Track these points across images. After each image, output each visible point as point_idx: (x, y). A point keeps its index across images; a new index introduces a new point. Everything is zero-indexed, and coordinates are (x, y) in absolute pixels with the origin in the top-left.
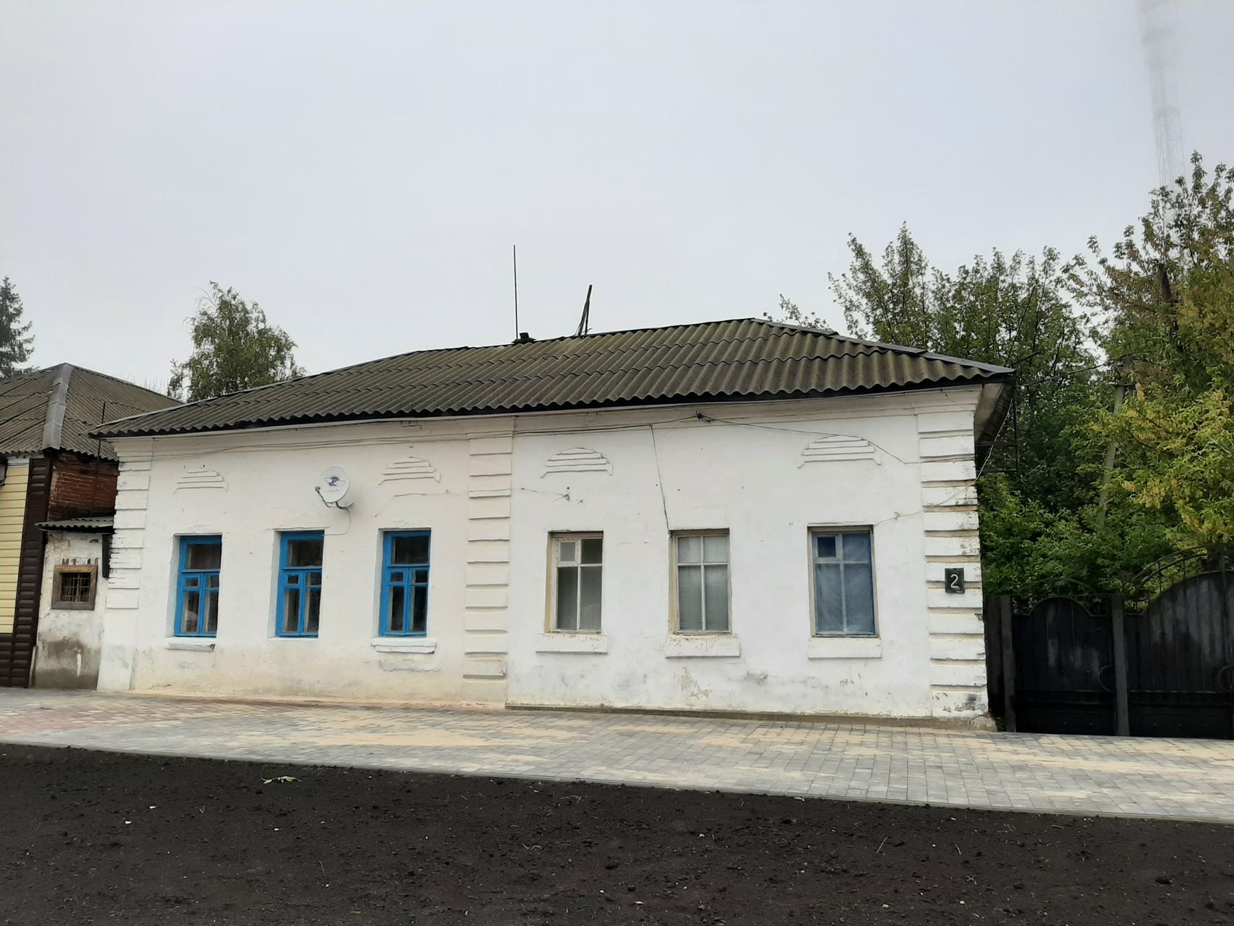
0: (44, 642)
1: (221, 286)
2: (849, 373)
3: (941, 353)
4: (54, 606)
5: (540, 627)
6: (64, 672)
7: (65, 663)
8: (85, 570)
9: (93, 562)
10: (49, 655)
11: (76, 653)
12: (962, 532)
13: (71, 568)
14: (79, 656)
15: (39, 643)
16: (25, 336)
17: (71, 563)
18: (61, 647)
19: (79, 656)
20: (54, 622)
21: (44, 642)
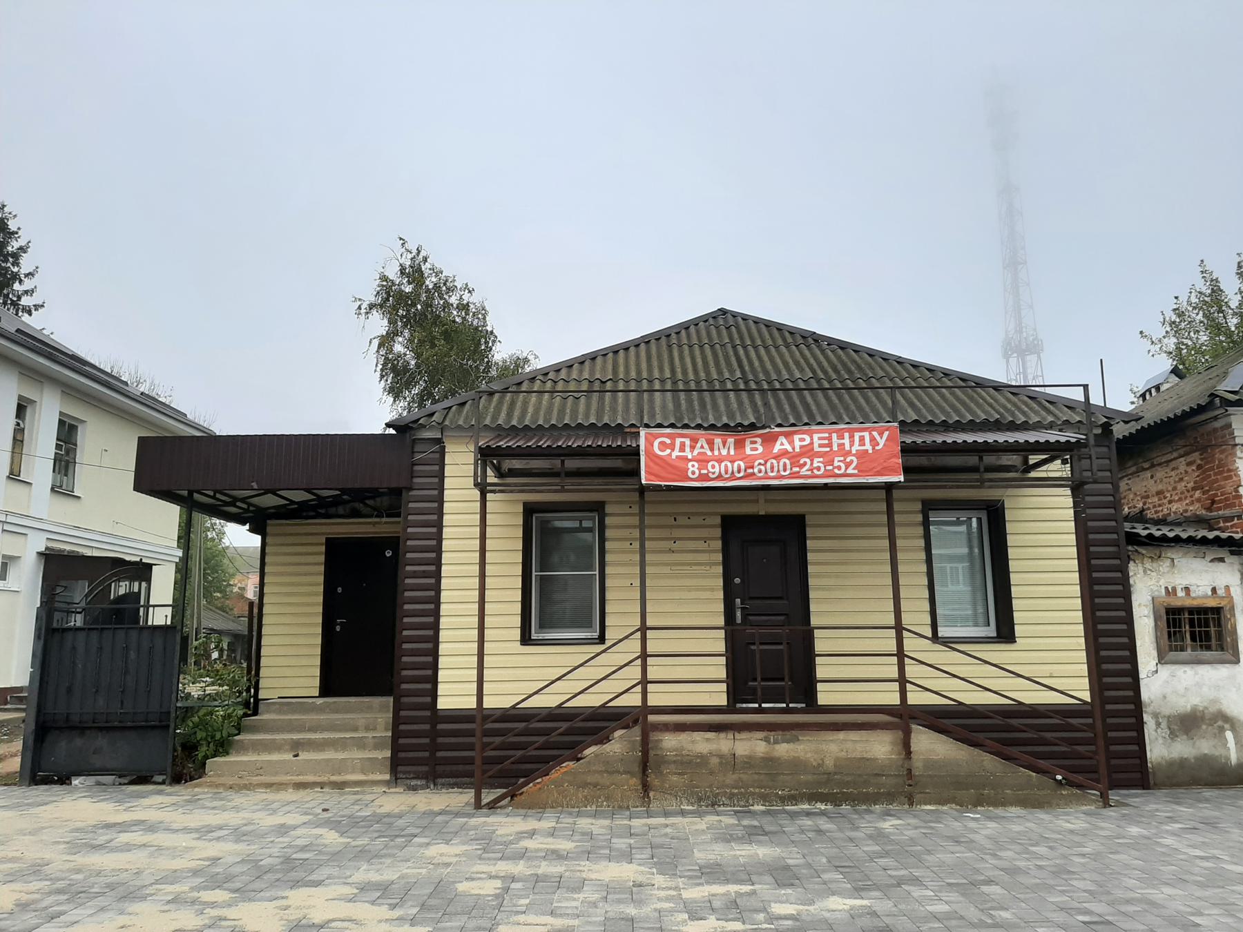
0: (1156, 716)
1: (409, 246)
2: (577, 411)
3: (438, 401)
4: (1162, 659)
5: (1223, 671)
6: (1204, 760)
7: (1204, 746)
8: (1212, 603)
9: (1221, 592)
10: (1173, 735)
11: (1222, 730)
12: (712, 564)
13: (1181, 600)
14: (1229, 735)
15: (1146, 717)
16: (28, 284)
17: (1181, 594)
18: (1188, 723)
19: (1229, 735)
20: (1167, 684)
21: (1156, 716)
